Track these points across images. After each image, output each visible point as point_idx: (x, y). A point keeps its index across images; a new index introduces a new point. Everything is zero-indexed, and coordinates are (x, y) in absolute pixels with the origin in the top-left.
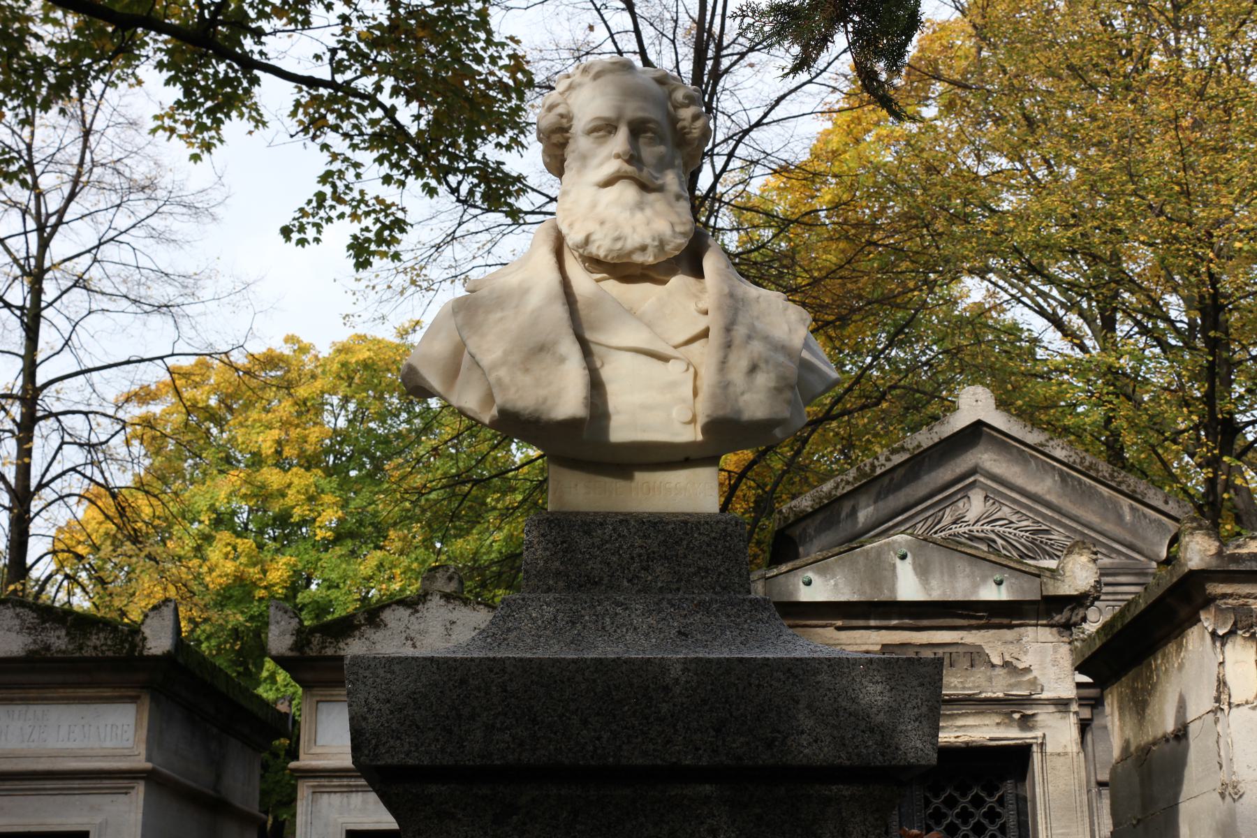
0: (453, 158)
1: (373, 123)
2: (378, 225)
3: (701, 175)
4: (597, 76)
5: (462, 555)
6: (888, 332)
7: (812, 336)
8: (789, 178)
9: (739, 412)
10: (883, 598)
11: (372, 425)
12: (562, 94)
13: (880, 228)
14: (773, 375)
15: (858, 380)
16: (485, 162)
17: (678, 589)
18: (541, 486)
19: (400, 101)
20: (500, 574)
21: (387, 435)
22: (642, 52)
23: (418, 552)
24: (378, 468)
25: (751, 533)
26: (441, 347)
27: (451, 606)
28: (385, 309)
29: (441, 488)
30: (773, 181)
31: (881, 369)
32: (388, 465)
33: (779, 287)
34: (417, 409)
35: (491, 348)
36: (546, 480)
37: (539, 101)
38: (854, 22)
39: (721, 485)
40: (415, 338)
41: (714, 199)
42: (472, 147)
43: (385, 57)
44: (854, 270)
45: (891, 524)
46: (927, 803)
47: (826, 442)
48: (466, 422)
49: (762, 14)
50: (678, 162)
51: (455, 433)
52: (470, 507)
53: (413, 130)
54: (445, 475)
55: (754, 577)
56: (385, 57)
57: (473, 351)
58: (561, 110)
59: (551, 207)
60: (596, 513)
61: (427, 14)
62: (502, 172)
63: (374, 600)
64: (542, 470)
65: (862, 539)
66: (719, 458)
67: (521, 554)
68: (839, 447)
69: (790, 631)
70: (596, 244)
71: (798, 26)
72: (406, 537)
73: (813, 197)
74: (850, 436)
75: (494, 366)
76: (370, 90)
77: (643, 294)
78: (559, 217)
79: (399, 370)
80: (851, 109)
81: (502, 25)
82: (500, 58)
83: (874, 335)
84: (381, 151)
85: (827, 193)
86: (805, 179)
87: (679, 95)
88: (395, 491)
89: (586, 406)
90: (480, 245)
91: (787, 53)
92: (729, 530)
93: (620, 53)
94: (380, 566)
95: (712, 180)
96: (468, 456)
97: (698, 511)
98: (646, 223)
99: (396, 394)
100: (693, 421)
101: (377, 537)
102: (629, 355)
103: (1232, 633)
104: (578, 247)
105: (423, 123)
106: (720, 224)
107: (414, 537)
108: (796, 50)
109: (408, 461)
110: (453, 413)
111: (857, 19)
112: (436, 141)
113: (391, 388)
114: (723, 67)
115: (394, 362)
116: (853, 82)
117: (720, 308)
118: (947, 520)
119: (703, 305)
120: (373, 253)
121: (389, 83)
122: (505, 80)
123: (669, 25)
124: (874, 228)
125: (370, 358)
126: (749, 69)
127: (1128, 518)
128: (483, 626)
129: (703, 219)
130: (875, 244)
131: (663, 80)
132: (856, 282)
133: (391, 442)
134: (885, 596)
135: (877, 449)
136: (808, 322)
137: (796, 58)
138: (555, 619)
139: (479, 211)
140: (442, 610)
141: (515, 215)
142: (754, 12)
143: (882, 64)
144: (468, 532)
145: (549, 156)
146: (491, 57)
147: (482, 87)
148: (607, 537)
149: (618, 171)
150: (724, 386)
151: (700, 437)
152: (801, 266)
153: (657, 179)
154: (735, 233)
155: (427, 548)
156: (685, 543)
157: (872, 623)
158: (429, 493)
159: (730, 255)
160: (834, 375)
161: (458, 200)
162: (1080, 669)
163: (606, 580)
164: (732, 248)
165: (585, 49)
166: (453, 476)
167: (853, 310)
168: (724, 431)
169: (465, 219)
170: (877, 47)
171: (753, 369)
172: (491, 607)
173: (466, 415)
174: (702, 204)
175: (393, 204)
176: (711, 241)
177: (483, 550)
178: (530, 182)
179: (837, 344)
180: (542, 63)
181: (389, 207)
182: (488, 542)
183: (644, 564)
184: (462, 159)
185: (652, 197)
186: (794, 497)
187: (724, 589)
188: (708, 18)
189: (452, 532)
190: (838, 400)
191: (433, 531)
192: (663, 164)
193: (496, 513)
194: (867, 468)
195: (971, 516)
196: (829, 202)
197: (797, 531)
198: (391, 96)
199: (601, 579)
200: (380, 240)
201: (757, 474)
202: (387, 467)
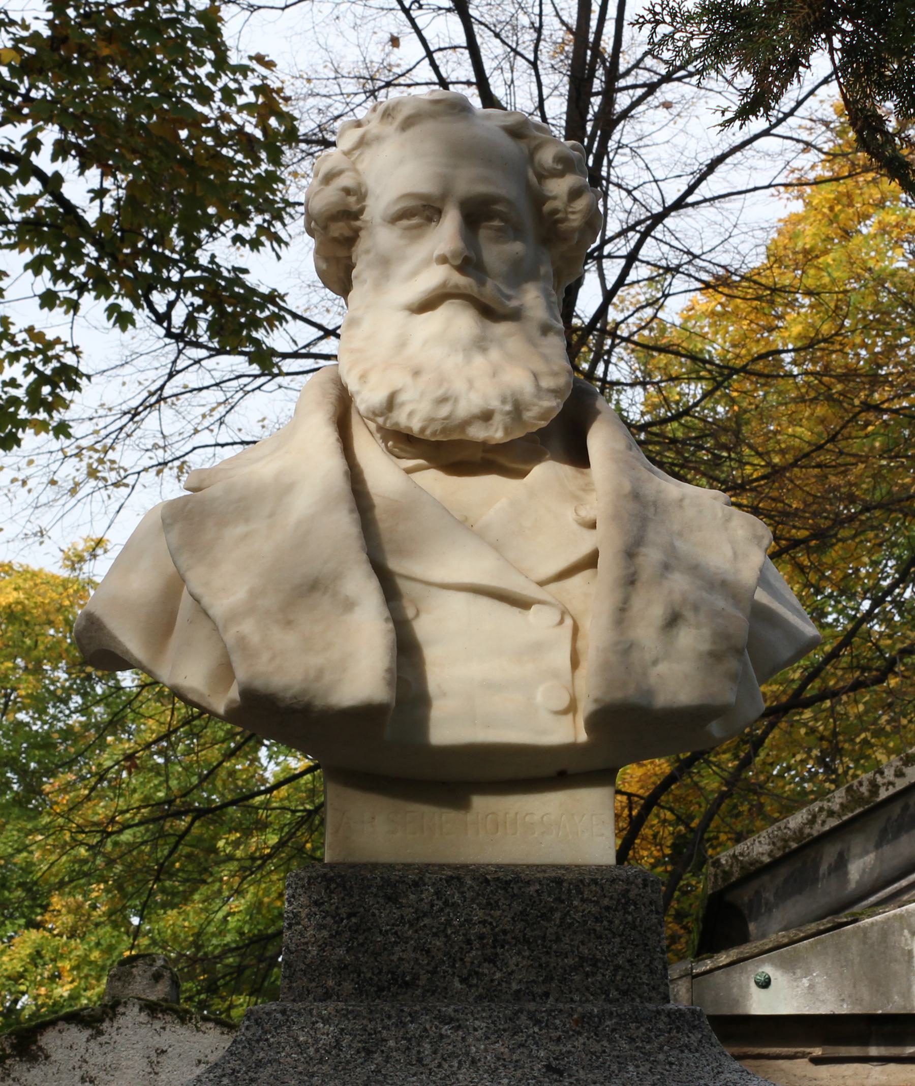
0: (161, 262)
1: (24, 202)
2: (33, 376)
3: (582, 292)
4: (409, 123)
5: (175, 936)
6: (899, 558)
7: (771, 564)
8: (731, 297)
9: (650, 693)
10: (891, 1009)
11: (22, 716)
12: (347, 153)
13: (885, 380)
14: (706, 631)
15: (848, 639)
16: (213, 272)
17: (547, 995)
18: (312, 820)
19: (69, 167)
20: (240, 969)
21: (48, 734)
22: (482, 83)
23: (101, 931)
24: (32, 788)
25: (668, 898)
26: (143, 584)
27: (158, 1025)
28: (45, 519)
29: (140, 823)
30: (702, 301)
31: (887, 620)
32: (49, 785)
33: (714, 481)
34: (99, 690)
35: (228, 584)
36: (319, 809)
37: (306, 165)
38: (844, 33)
39: (617, 816)
40: (98, 569)
41: (604, 332)
42: (192, 244)
43: (42, 91)
44: (841, 453)
47: (793, 745)
48: (183, 711)
49: (689, 18)
50: (545, 269)
51: (164, 729)
52: (189, 856)
53: (91, 216)
54: (146, 801)
55: (674, 972)
56: (42, 91)
57: (198, 590)
59: (328, 346)
60: (407, 866)
61: (116, 19)
62: (243, 285)
63: (26, 1014)
64: (312, 793)
65: (856, 909)
66: (614, 771)
67: (279, 933)
68: (816, 752)
69: (737, 1065)
70: (407, 409)
71: (749, 38)
72: (80, 906)
73: (771, 329)
74: (835, 734)
75: (234, 616)
76: (19, 146)
77: (486, 495)
78: (344, 363)
79: (67, 622)
80: (836, 179)
81: (241, 34)
82: (240, 91)
83: (875, 564)
84: (37, 251)
85: (795, 323)
86: (758, 298)
87: (547, 156)
88: (62, 828)
89: (389, 684)
90: (205, 410)
91: (731, 84)
92: (632, 895)
93: (444, 83)
94: (37, 956)
95: (599, 300)
96: (186, 769)
97: (580, 861)
98: (483, 372)
99: (63, 664)
100: (571, 708)
101: (31, 908)
102: (462, 598)
104: (375, 414)
105: (108, 202)
106: (614, 374)
107: (94, 907)
108: (746, 79)
109: (83, 778)
110: (160, 696)
111: (848, 27)
112: (131, 233)
113: (55, 654)
114: (618, 108)
115: (60, 609)
116: (841, 134)
117: (616, 517)
119: (587, 513)
120: (24, 424)
121: (50, 134)
122: (249, 129)
123: (528, 37)
124: (875, 381)
125: (18, 603)
126: (662, 111)
128: (213, 1058)
129: (585, 366)
130: (878, 409)
131: (519, 130)
132: (845, 473)
133: (55, 746)
135: (881, 756)
136: (766, 542)
137: (745, 94)
138: (338, 1045)
139: (203, 353)
140: (143, 1031)
141: (265, 359)
142: (673, 15)
143: (889, 105)
144: (187, 898)
145: (327, 259)
146: (225, 90)
147: (209, 141)
148: (426, 908)
149: (444, 284)
150: (623, 650)
151: (583, 737)
152: (750, 447)
153: (509, 298)
154: (639, 389)
155: (116, 926)
156: (558, 915)
157: (874, 1051)
158: (120, 832)
159: (632, 427)
160: (810, 630)
161: (169, 334)
163: (423, 981)
164: (634, 415)
165: (385, 77)
166: (160, 803)
167: (839, 521)
168: (624, 727)
169: (180, 365)
170: (882, 75)
171: (673, 621)
172: (227, 1025)
173: (182, 698)
174: (583, 341)
175: (58, 341)
176: (600, 403)
177: (212, 929)
178: (291, 303)
179: (813, 577)
180: (312, 101)
181: (51, 345)
182: (220, 915)
183: (489, 951)
184: (175, 263)
185: (501, 329)
186: (739, 838)
187: (624, 993)
188: (594, 24)
189: (158, 898)
190: (815, 672)
191: (125, 896)
192: (520, 274)
193: (233, 866)
194: (864, 789)
196: (800, 337)
197: (744, 896)
198: (54, 159)
199: (416, 977)
200: (35, 401)
201: (677, 799)
202: (47, 788)
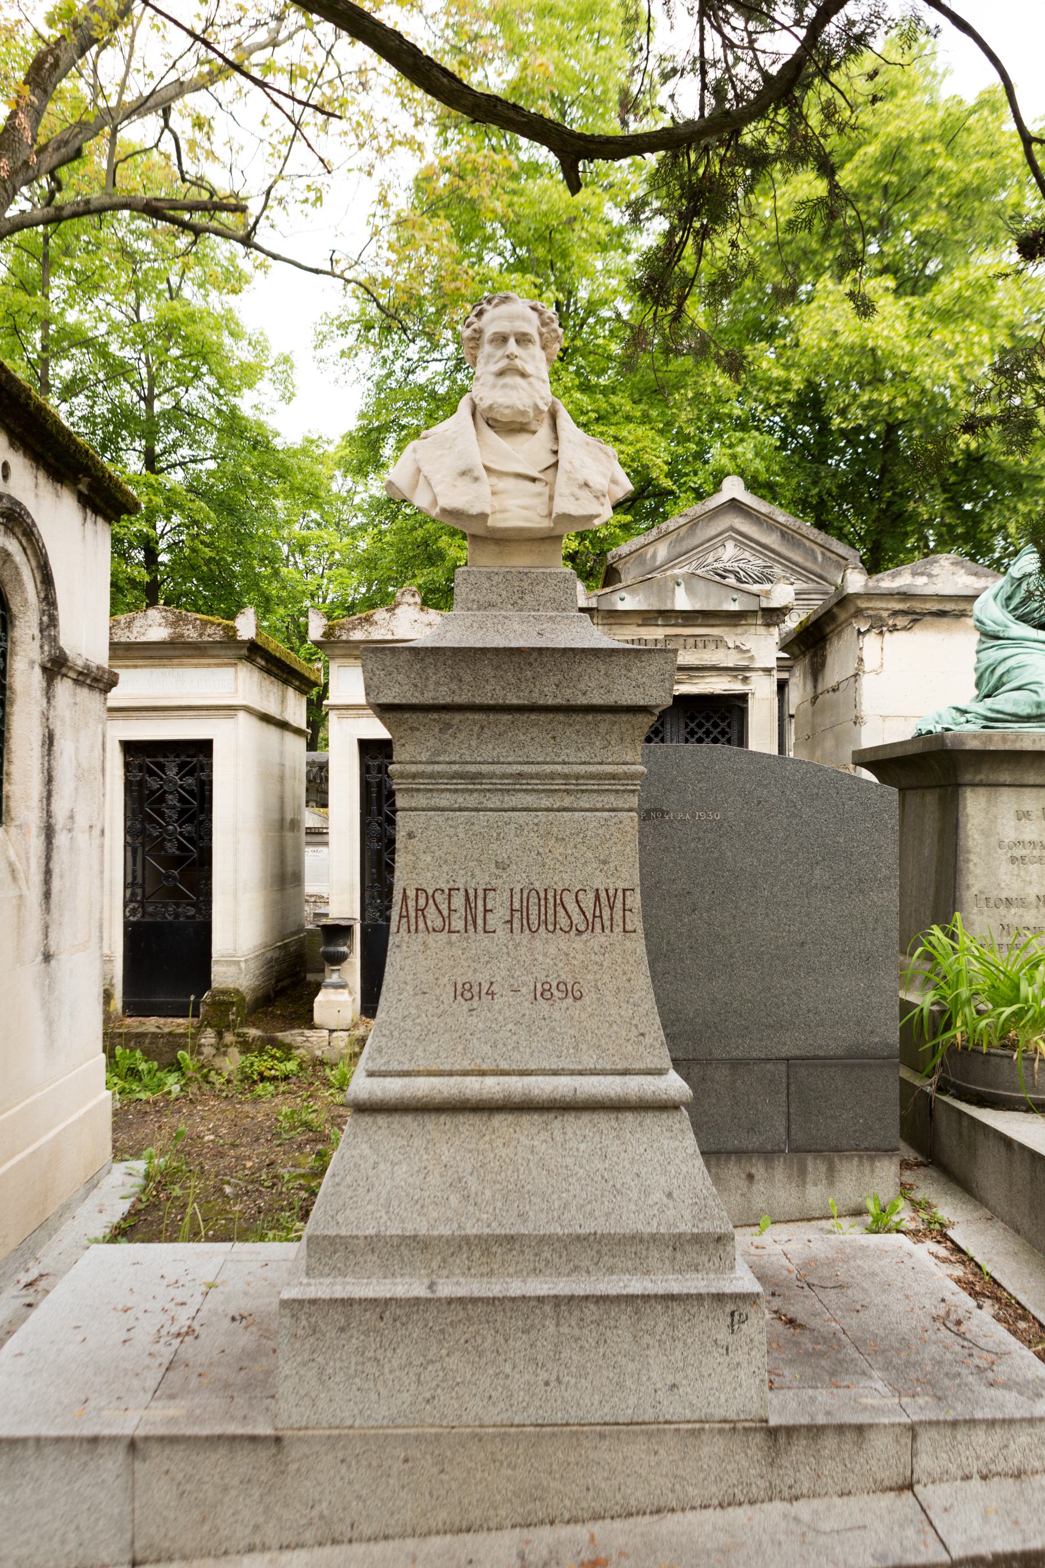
46: (687, 726)
103: (868, 631)
118: (710, 560)
127: (820, 559)
134: (668, 607)
162: (782, 649)
195: (725, 558)
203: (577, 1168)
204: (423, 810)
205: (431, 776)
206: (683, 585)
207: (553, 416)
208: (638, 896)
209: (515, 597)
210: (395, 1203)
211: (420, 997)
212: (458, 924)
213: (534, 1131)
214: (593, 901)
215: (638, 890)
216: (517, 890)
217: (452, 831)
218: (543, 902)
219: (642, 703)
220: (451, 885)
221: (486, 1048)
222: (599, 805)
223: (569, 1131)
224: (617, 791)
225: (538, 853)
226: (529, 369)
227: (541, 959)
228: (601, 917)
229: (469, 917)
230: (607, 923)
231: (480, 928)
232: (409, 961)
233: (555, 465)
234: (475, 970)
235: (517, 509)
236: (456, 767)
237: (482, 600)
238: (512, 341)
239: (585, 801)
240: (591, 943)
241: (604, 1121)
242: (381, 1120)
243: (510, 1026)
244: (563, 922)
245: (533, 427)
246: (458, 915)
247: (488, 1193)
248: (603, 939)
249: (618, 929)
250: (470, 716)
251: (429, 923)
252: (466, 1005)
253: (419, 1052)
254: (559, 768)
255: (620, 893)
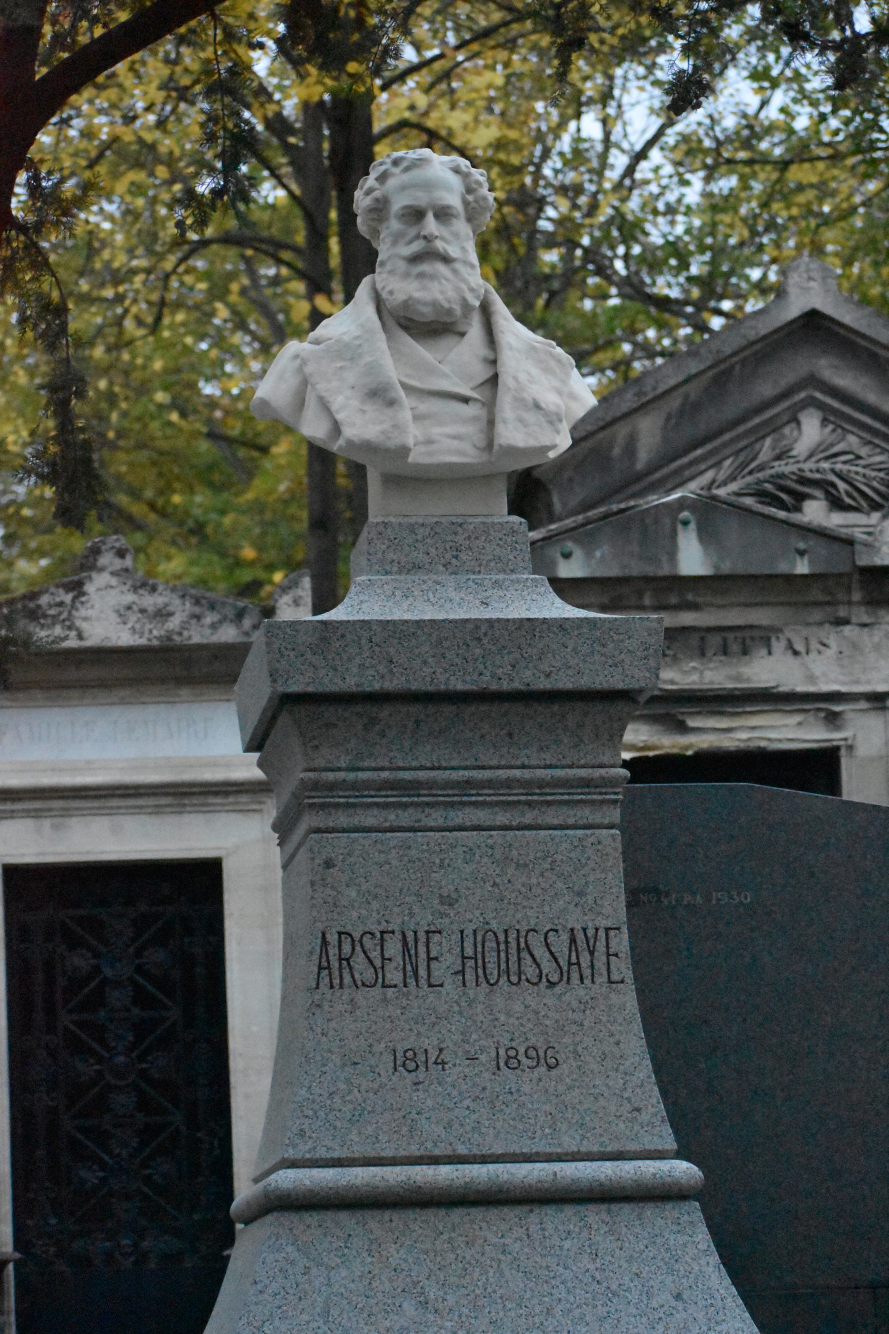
45: (685, 460)
58: (377, 194)
203: (561, 1269)
204: (344, 831)
205: (354, 786)
206: (692, 526)
207: (486, 309)
208: (626, 936)
209: (448, 556)
210: (335, 1312)
211: (349, 1069)
212: (394, 976)
213: (504, 1226)
214: (567, 944)
215: (625, 929)
216: (468, 932)
217: (382, 858)
218: (502, 947)
219: (621, 686)
220: (384, 926)
221: (439, 1130)
222: (571, 821)
223: (550, 1227)
224: (592, 802)
225: (495, 884)
226: (453, 251)
227: (503, 1018)
228: (578, 964)
229: (409, 968)
230: (587, 972)
231: (423, 982)
232: (333, 1024)
233: (494, 380)
234: (419, 1034)
235: (441, 438)
236: (385, 774)
237: (404, 560)
238: (430, 218)
239: (552, 816)
240: (567, 998)
241: (594, 1215)
242: (311, 1218)
243: (466, 1103)
244: (530, 971)
245: (461, 329)
246: (393, 964)
247: (451, 1300)
248: (582, 992)
249: (602, 979)
250: (404, 709)
251: (357, 976)
252: (410, 1078)
253: (354, 1136)
254: (517, 773)
255: (602, 934)
